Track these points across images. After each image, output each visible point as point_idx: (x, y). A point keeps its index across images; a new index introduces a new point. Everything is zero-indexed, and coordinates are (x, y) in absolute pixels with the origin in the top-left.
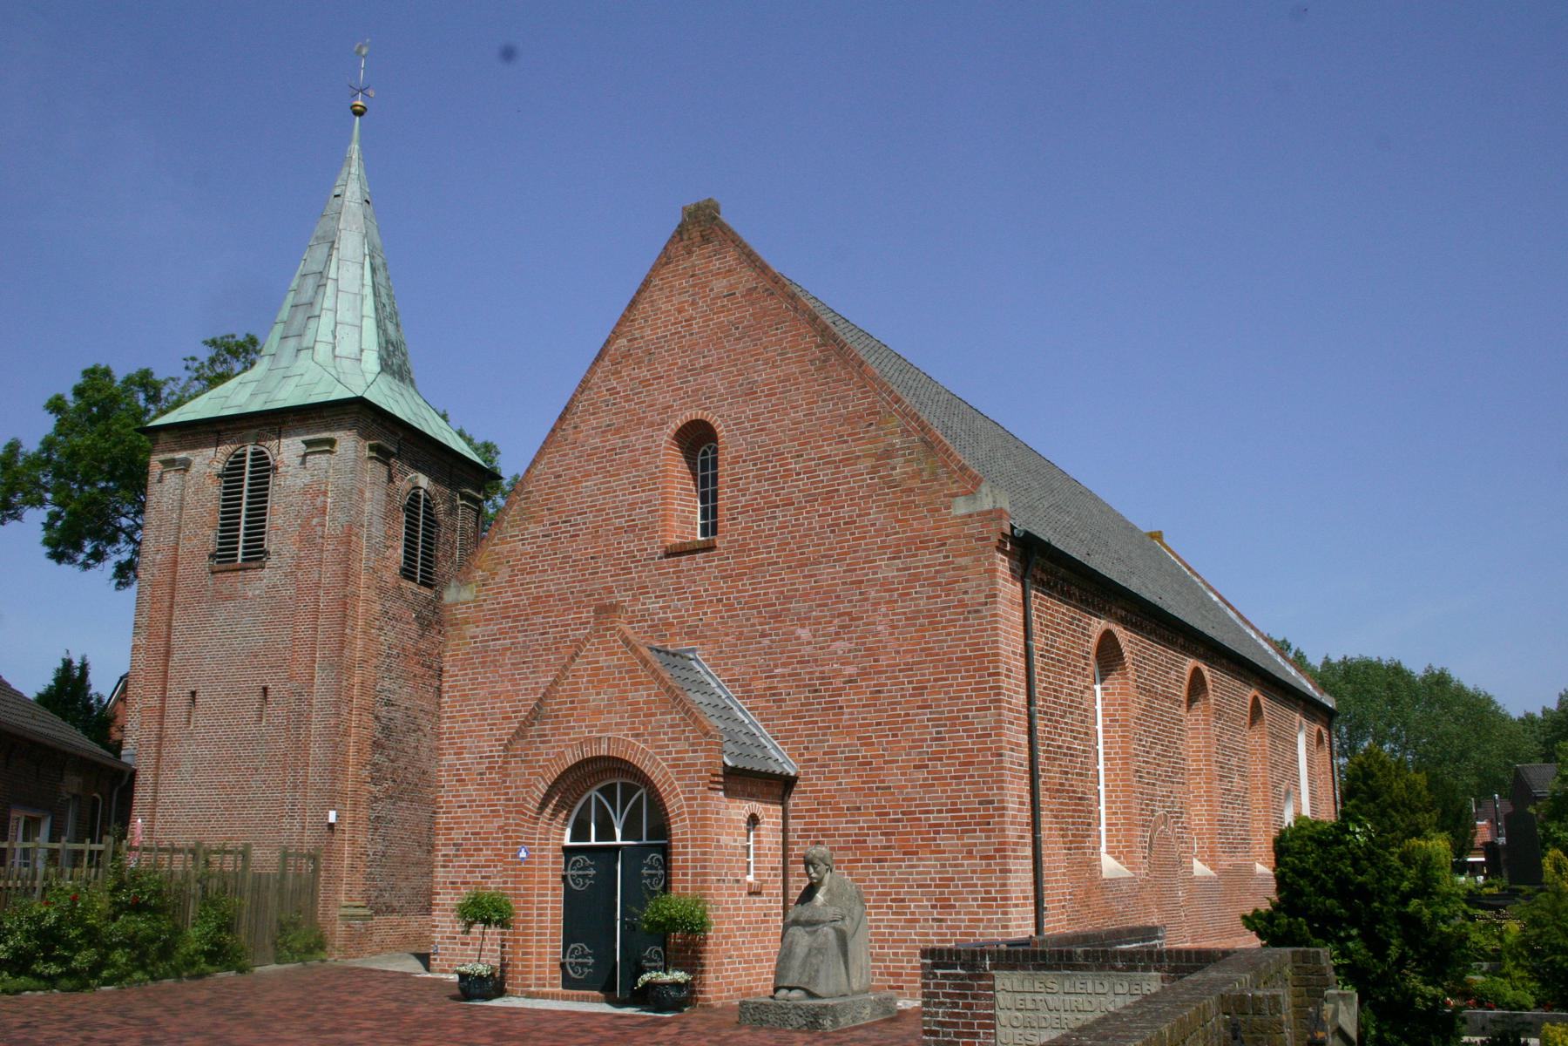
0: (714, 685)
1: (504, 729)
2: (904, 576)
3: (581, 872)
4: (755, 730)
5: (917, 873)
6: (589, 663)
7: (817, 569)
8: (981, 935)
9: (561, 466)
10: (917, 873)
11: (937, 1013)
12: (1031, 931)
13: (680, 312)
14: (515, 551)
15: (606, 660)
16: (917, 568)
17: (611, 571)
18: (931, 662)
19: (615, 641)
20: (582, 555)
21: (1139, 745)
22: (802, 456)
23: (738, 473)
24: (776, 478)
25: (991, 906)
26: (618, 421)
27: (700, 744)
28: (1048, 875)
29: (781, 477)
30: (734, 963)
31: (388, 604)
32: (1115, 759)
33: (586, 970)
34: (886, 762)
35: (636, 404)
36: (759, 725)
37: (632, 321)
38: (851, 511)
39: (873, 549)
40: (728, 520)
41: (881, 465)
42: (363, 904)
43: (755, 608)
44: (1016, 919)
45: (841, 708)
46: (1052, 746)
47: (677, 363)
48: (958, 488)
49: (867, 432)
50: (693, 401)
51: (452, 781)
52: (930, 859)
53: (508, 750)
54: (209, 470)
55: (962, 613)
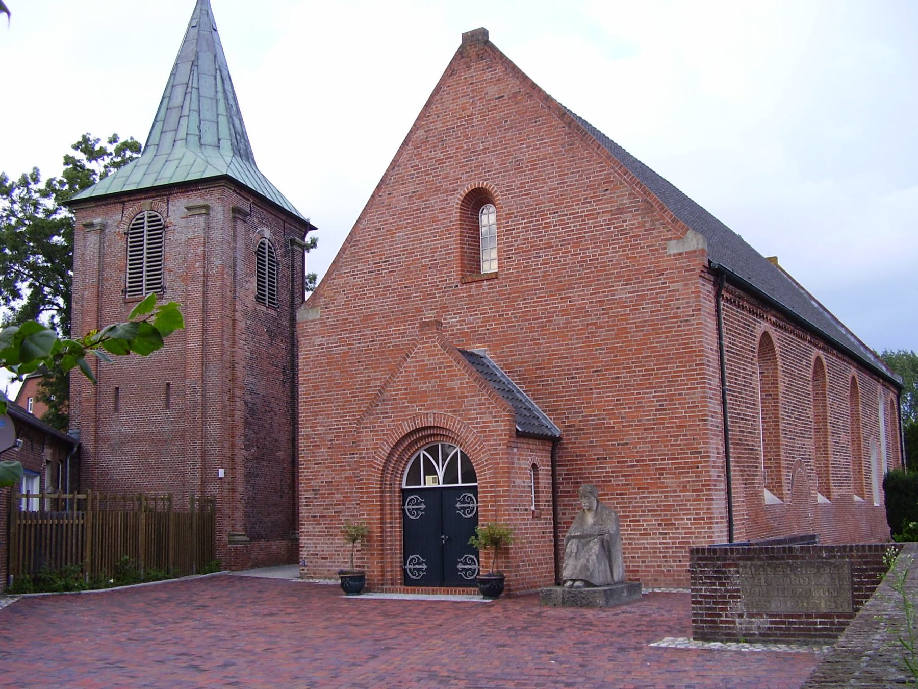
0: (499, 375)
1: (346, 409)
2: (634, 297)
4: (529, 406)
5: (648, 502)
6: (417, 362)
7: (572, 293)
8: (693, 543)
9: (379, 222)
10: (648, 502)
11: (701, 589)
12: (724, 540)
13: (463, 111)
14: (348, 283)
15: (429, 360)
16: (644, 291)
17: (420, 296)
18: (655, 356)
19: (435, 346)
20: (398, 285)
21: (785, 412)
22: (557, 212)
23: (511, 226)
24: (539, 229)
25: (700, 523)
26: (421, 189)
27: (501, 416)
28: (734, 503)
29: (543, 228)
30: (526, 565)
31: (249, 322)
32: (769, 422)
34: (623, 426)
35: (433, 177)
36: (532, 402)
37: (428, 116)
38: (595, 251)
39: (611, 278)
40: (505, 259)
41: (615, 219)
42: (243, 533)
43: (526, 320)
44: (717, 532)
45: (591, 389)
46: (735, 413)
47: (462, 147)
48: (671, 234)
49: (605, 195)
50: (476, 174)
51: (310, 446)
52: (657, 492)
53: (360, 423)
54: (118, 230)
55: (677, 322)
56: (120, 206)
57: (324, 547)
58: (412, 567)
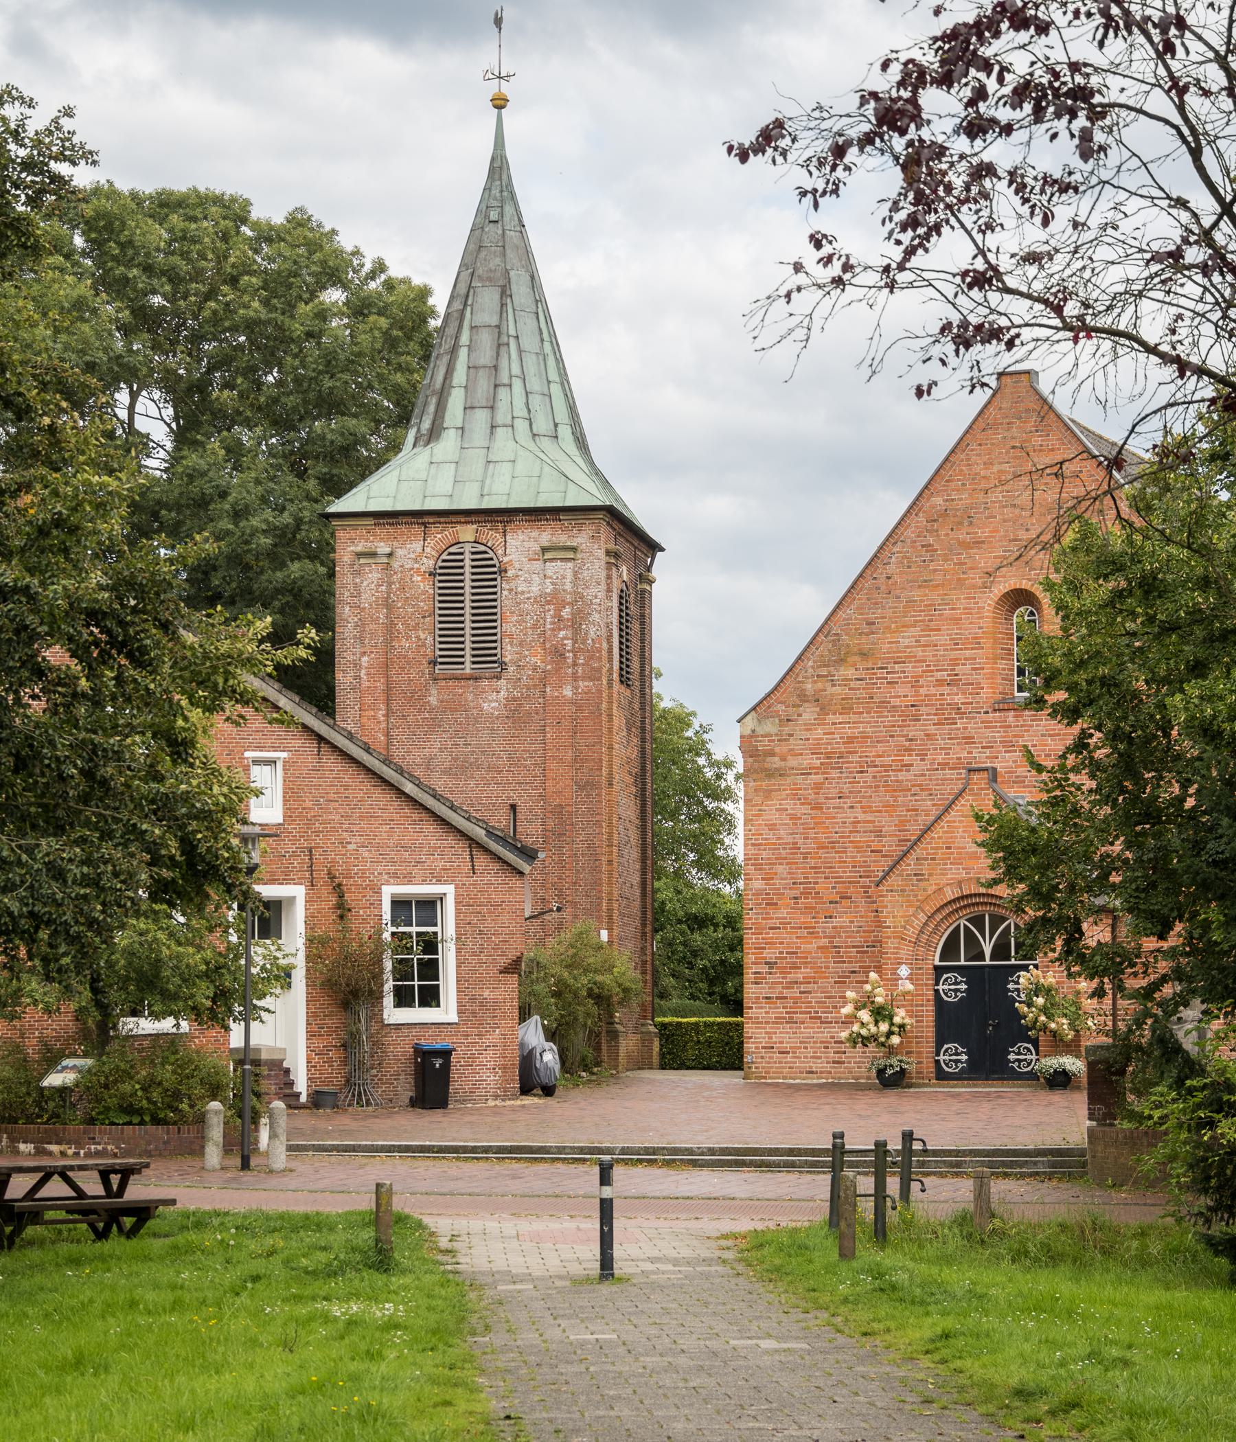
3: (953, 987)
33: (960, 1065)
54: (416, 566)
56: (418, 529)
57: (784, 1036)
58: (947, 1058)
